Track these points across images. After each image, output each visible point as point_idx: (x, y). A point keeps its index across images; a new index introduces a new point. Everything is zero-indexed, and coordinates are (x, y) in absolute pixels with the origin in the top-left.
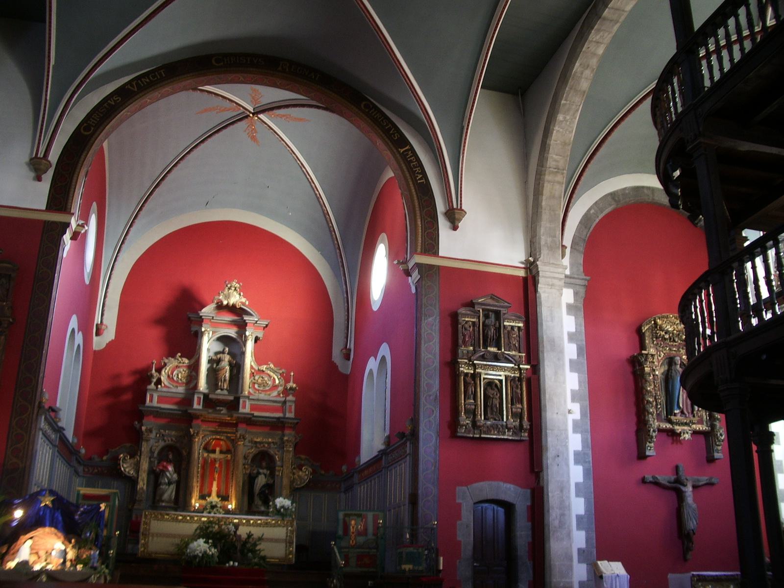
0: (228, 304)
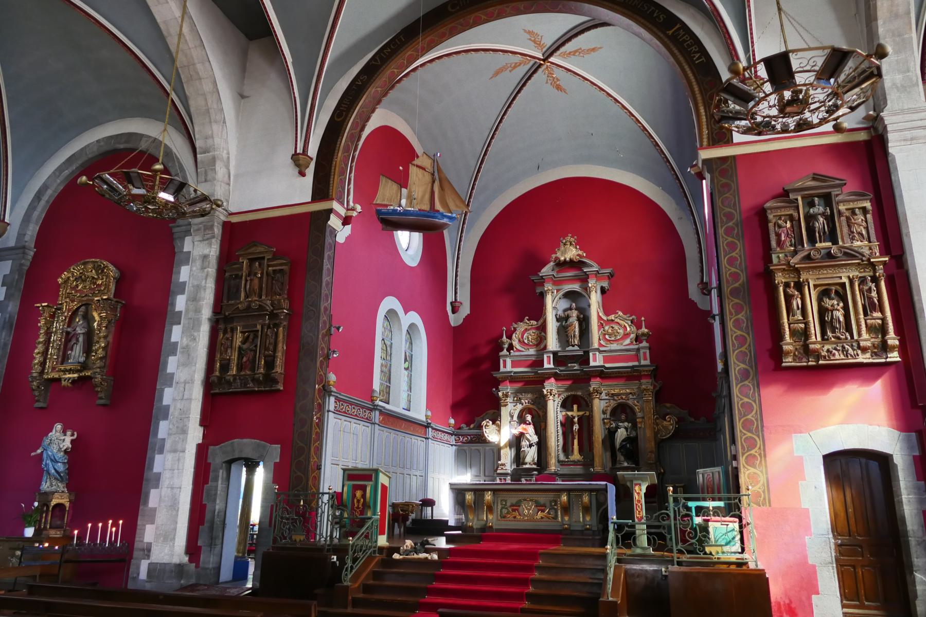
0: (565, 259)
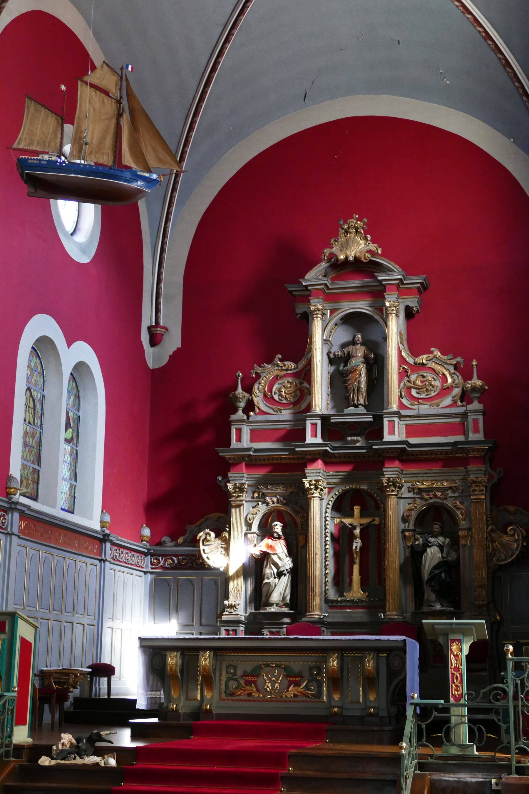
0: (347, 258)
